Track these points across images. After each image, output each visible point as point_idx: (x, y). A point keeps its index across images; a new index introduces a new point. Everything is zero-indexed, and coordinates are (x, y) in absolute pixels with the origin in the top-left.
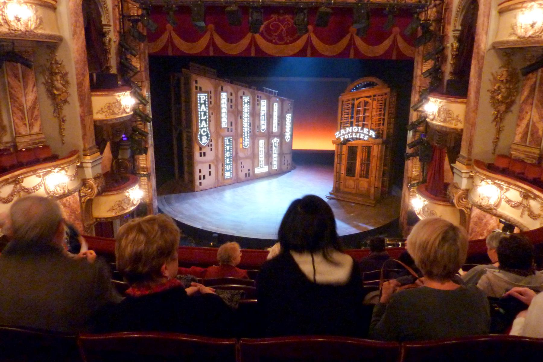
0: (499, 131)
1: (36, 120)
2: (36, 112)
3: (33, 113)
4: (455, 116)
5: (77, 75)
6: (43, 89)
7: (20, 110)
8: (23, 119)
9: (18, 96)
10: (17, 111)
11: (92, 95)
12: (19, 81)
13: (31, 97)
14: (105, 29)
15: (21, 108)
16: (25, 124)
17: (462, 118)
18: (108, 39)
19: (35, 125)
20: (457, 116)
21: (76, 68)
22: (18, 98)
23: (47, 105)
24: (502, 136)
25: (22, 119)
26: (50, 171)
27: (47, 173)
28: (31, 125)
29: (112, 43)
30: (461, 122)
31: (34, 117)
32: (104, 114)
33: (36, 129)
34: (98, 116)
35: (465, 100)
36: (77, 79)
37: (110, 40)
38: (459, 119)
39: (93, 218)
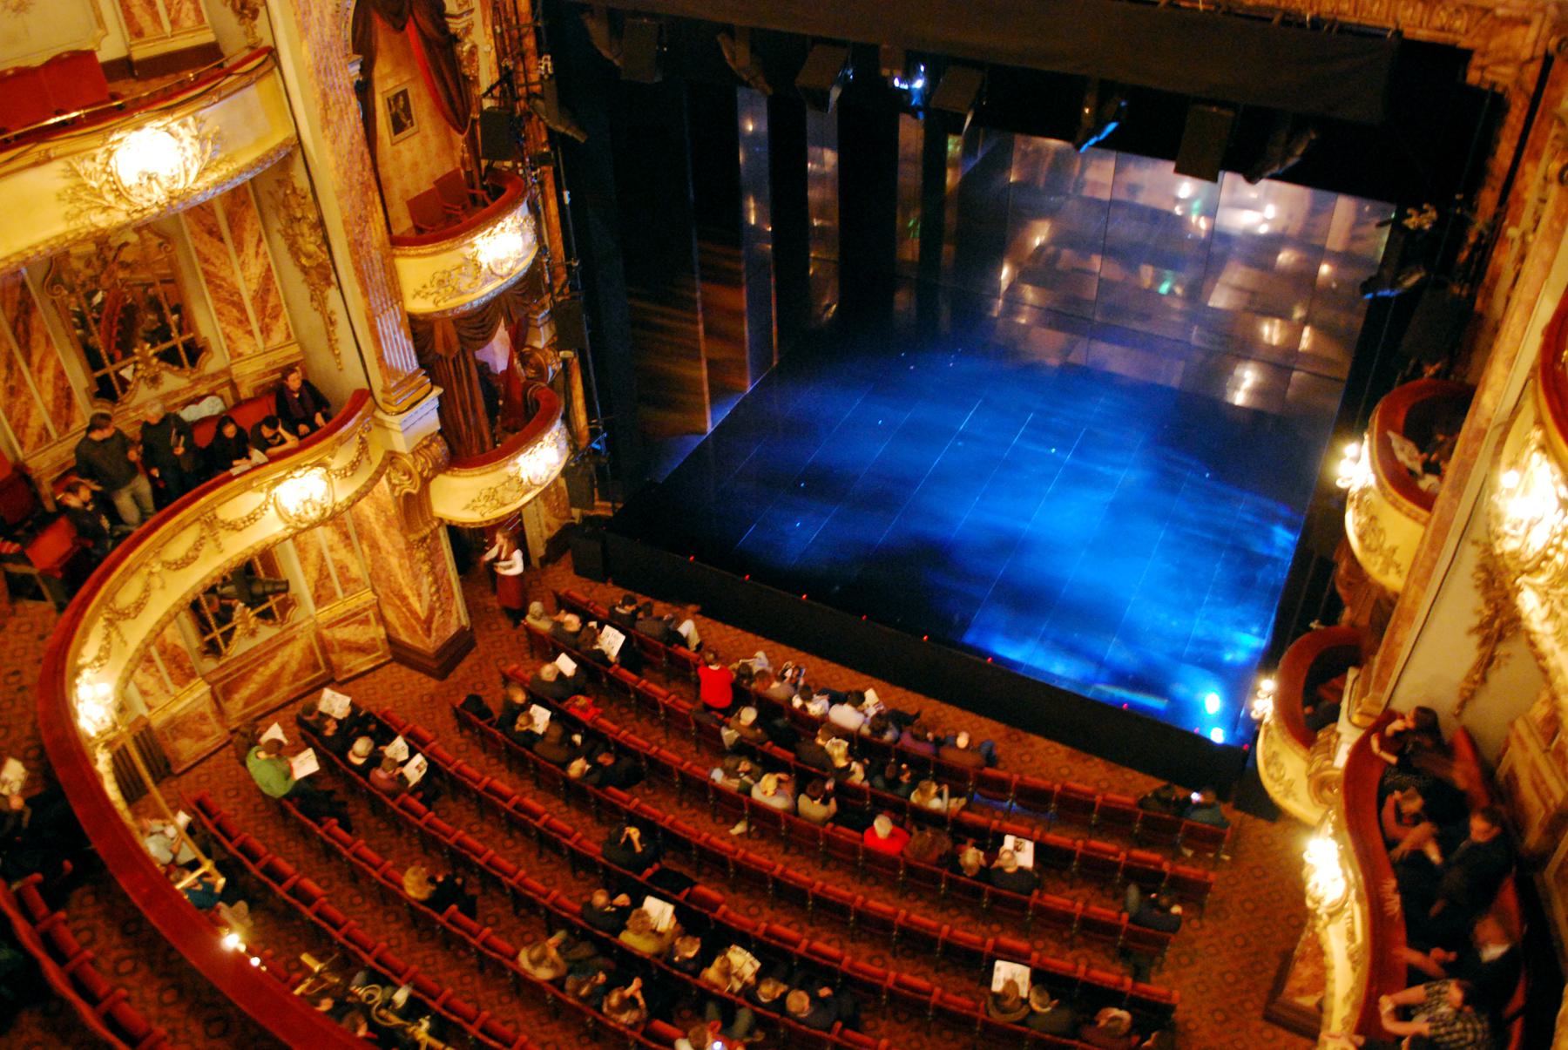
0: (1487, 663)
1: (276, 317)
2: (272, 301)
3: (265, 301)
4: (1386, 546)
5: (345, 222)
6: (280, 244)
7: (234, 304)
8: (243, 321)
9: (222, 274)
10: (226, 309)
11: (394, 256)
12: (221, 240)
13: (255, 269)
14: (455, 26)
15: (235, 298)
16: (250, 333)
17: (1404, 558)
18: (466, 48)
19: (275, 328)
20: (1394, 550)
21: (341, 208)
22: (224, 279)
23: (293, 284)
24: (1496, 677)
25: (240, 322)
26: (283, 478)
27: (277, 482)
28: (266, 331)
29: (481, 55)
30: (1399, 572)
31: (269, 311)
32: (431, 298)
33: (278, 337)
34: (419, 306)
35: (1424, 513)
36: (347, 233)
37: (473, 52)
38: (1397, 558)
39: (433, 518)
